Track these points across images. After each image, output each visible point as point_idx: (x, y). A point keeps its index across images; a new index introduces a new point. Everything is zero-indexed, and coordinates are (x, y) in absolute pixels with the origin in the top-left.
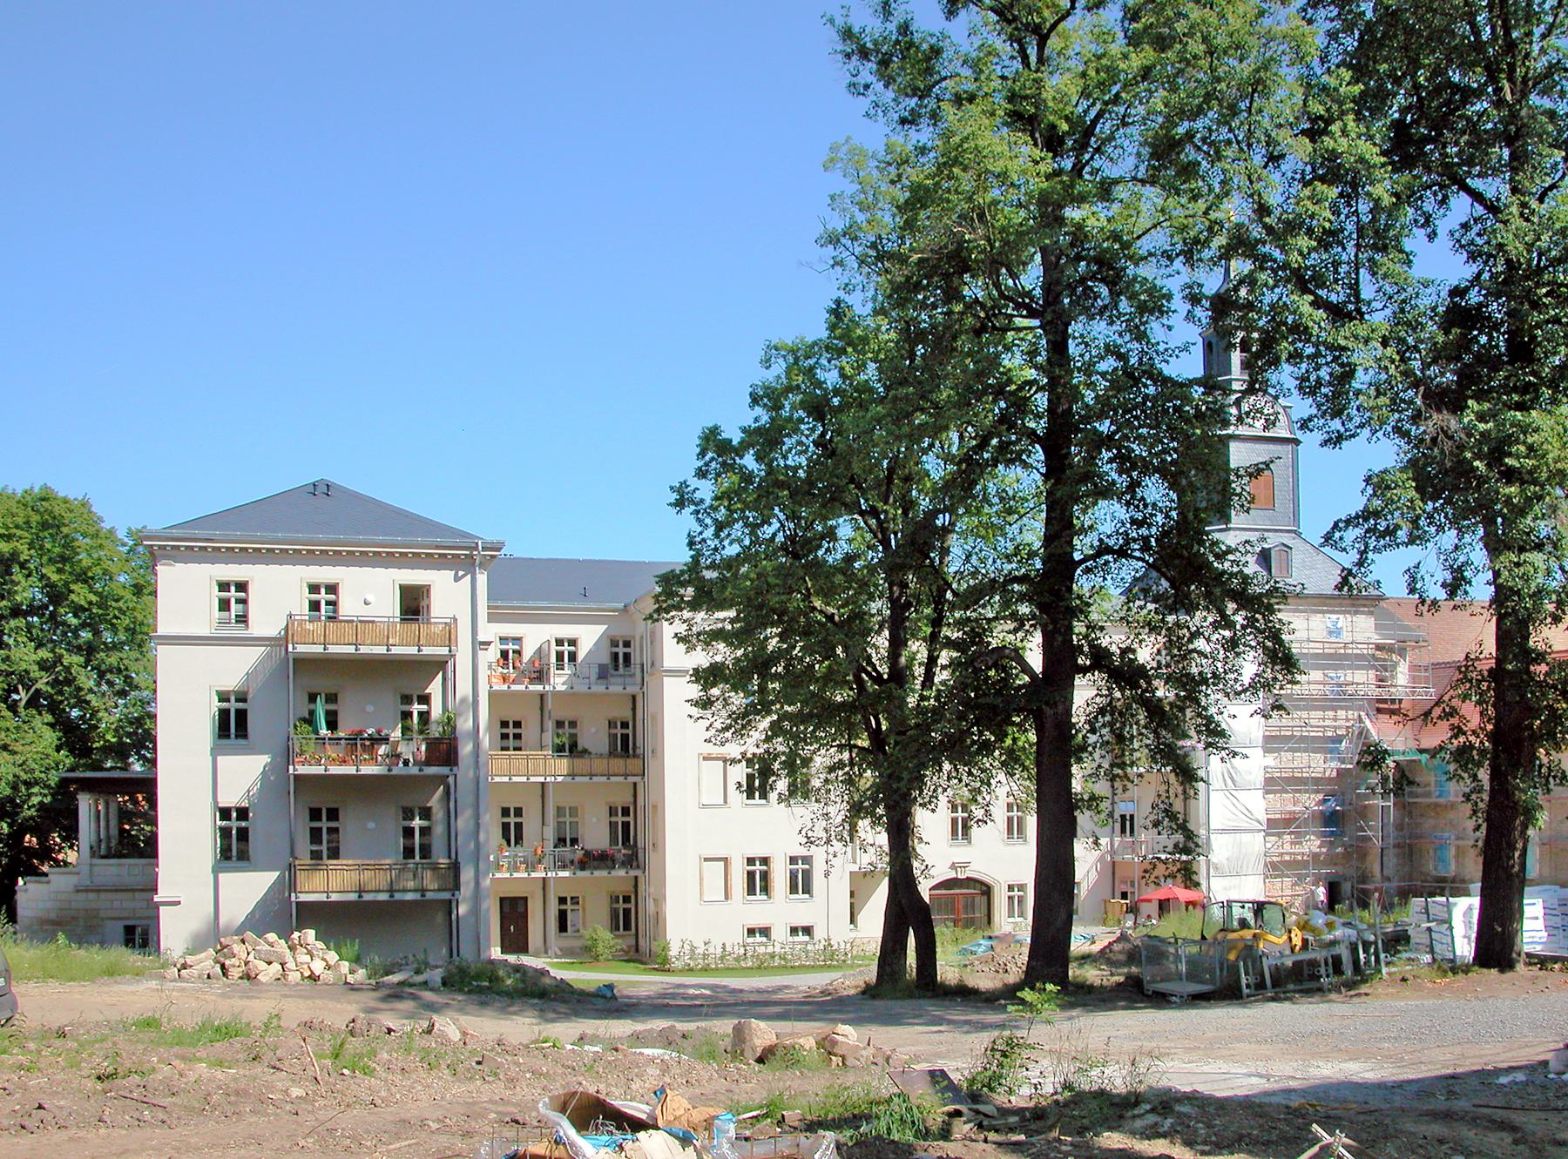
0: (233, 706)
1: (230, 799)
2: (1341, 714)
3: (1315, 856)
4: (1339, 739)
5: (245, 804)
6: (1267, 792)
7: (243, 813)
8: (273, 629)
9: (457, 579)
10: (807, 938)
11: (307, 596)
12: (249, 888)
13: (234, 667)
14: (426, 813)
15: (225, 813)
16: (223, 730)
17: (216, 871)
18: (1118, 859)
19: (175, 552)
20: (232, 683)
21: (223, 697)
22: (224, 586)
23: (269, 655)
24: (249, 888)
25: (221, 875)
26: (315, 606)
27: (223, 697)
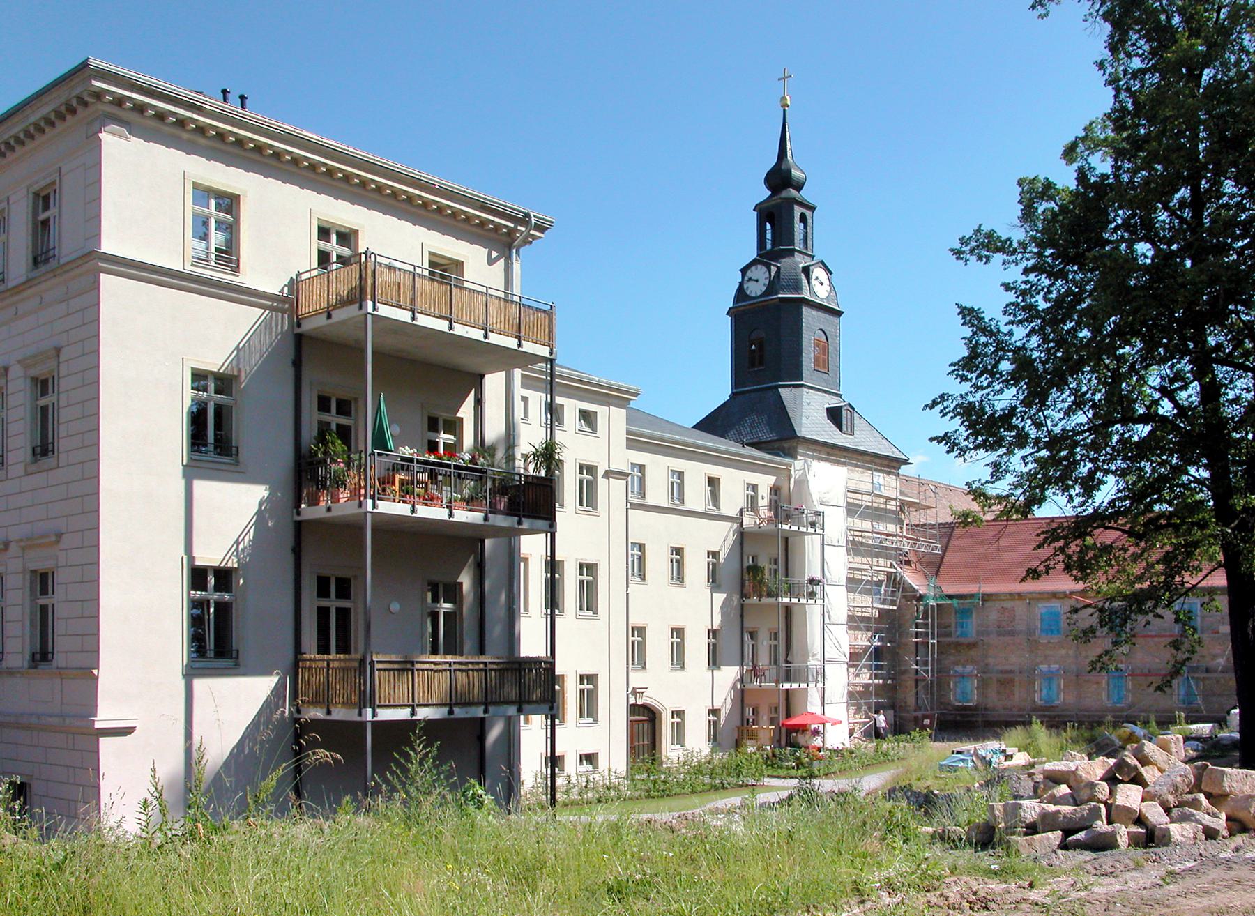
0: (211, 396)
1: (211, 554)
2: (882, 561)
3: (866, 686)
4: (879, 583)
5: (233, 563)
6: (850, 628)
7: (224, 576)
8: (274, 285)
9: (491, 262)
10: (590, 767)
11: (316, 244)
12: (236, 704)
13: (221, 334)
14: (453, 592)
15: (198, 576)
16: (197, 436)
17: (190, 673)
18: (748, 686)
19: (134, 117)
20: (215, 361)
21: (199, 377)
22: (203, 193)
23: (267, 324)
24: (236, 704)
25: (199, 684)
26: (324, 258)
27: (199, 377)
